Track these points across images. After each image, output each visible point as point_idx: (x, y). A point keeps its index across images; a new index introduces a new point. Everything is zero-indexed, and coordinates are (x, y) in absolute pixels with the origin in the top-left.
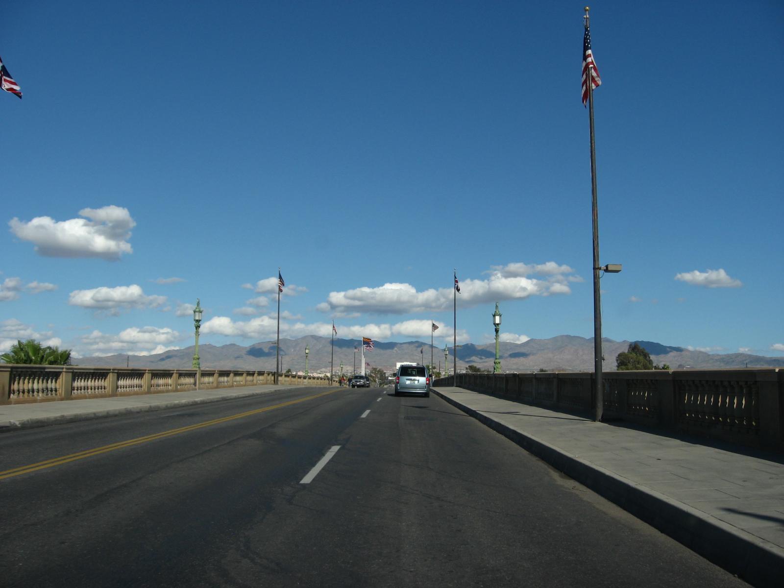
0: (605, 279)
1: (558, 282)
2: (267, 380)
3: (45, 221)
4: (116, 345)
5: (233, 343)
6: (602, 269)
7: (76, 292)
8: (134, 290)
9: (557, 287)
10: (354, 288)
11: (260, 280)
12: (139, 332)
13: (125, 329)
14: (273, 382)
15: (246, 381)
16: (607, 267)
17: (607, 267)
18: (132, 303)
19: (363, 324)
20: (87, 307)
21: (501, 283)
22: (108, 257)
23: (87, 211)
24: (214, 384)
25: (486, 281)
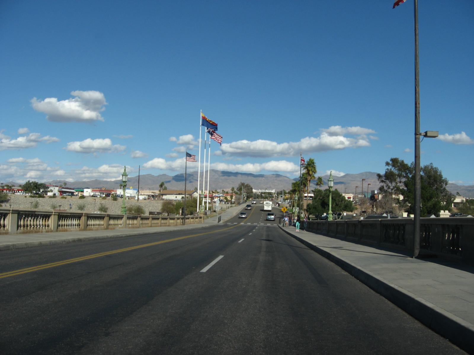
0: (424, 143)
1: (363, 139)
2: (177, 223)
3: (53, 100)
4: (95, 175)
5: (164, 174)
6: (422, 134)
7: (71, 143)
8: (106, 142)
9: (362, 142)
10: (236, 140)
11: (182, 135)
12: (109, 167)
13: (101, 165)
14: (182, 224)
15: (161, 223)
16: (426, 133)
17: (426, 133)
18: (104, 150)
19: (243, 163)
20: (77, 152)
21: (327, 139)
22: (90, 121)
23: (76, 93)
24: (137, 225)
25: (318, 138)
